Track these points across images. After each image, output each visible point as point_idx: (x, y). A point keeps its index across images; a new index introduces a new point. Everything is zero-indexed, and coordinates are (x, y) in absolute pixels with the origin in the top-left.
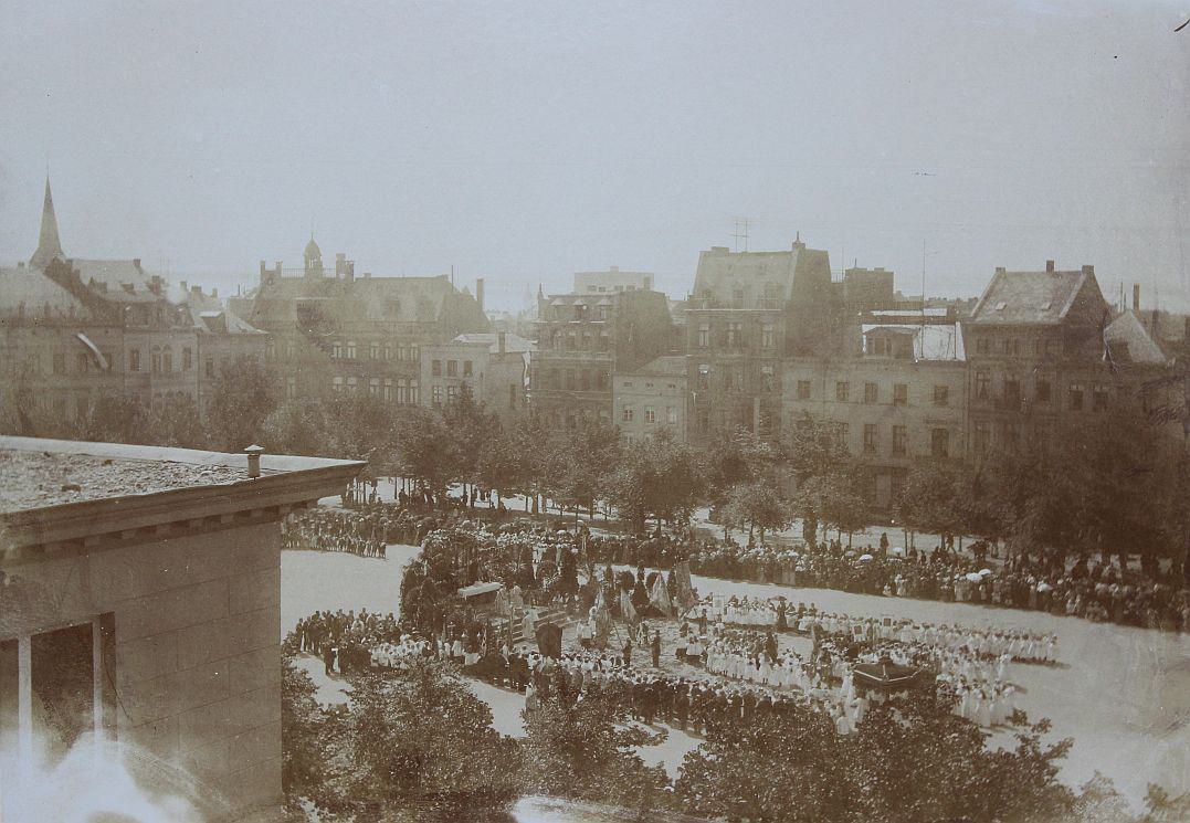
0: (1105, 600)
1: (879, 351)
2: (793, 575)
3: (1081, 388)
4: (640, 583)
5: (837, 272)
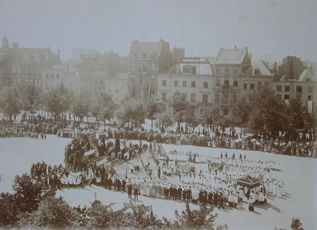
0: (278, 147)
1: (186, 72)
2: (180, 142)
3: (247, 83)
4: (141, 148)
5: (20, 47)
